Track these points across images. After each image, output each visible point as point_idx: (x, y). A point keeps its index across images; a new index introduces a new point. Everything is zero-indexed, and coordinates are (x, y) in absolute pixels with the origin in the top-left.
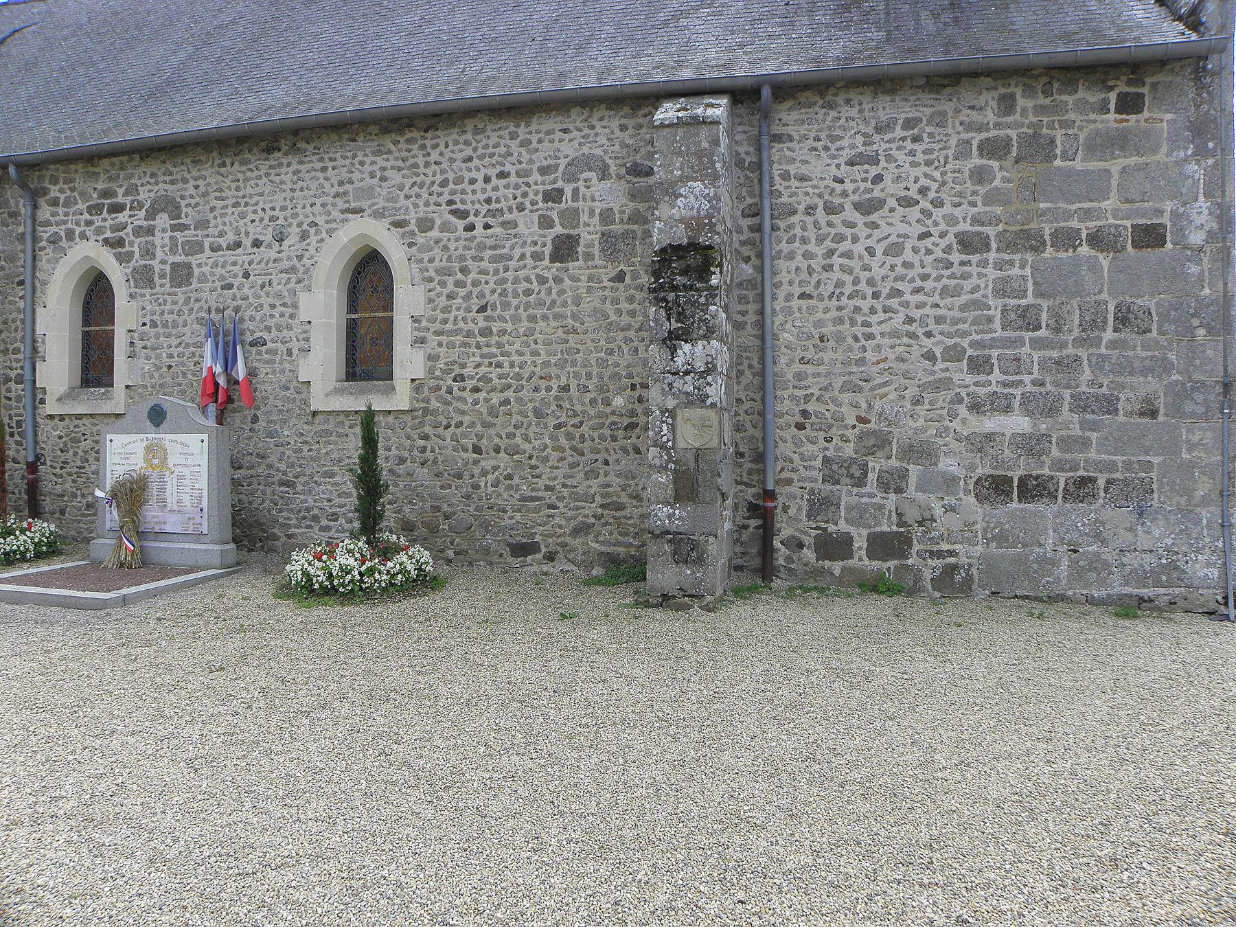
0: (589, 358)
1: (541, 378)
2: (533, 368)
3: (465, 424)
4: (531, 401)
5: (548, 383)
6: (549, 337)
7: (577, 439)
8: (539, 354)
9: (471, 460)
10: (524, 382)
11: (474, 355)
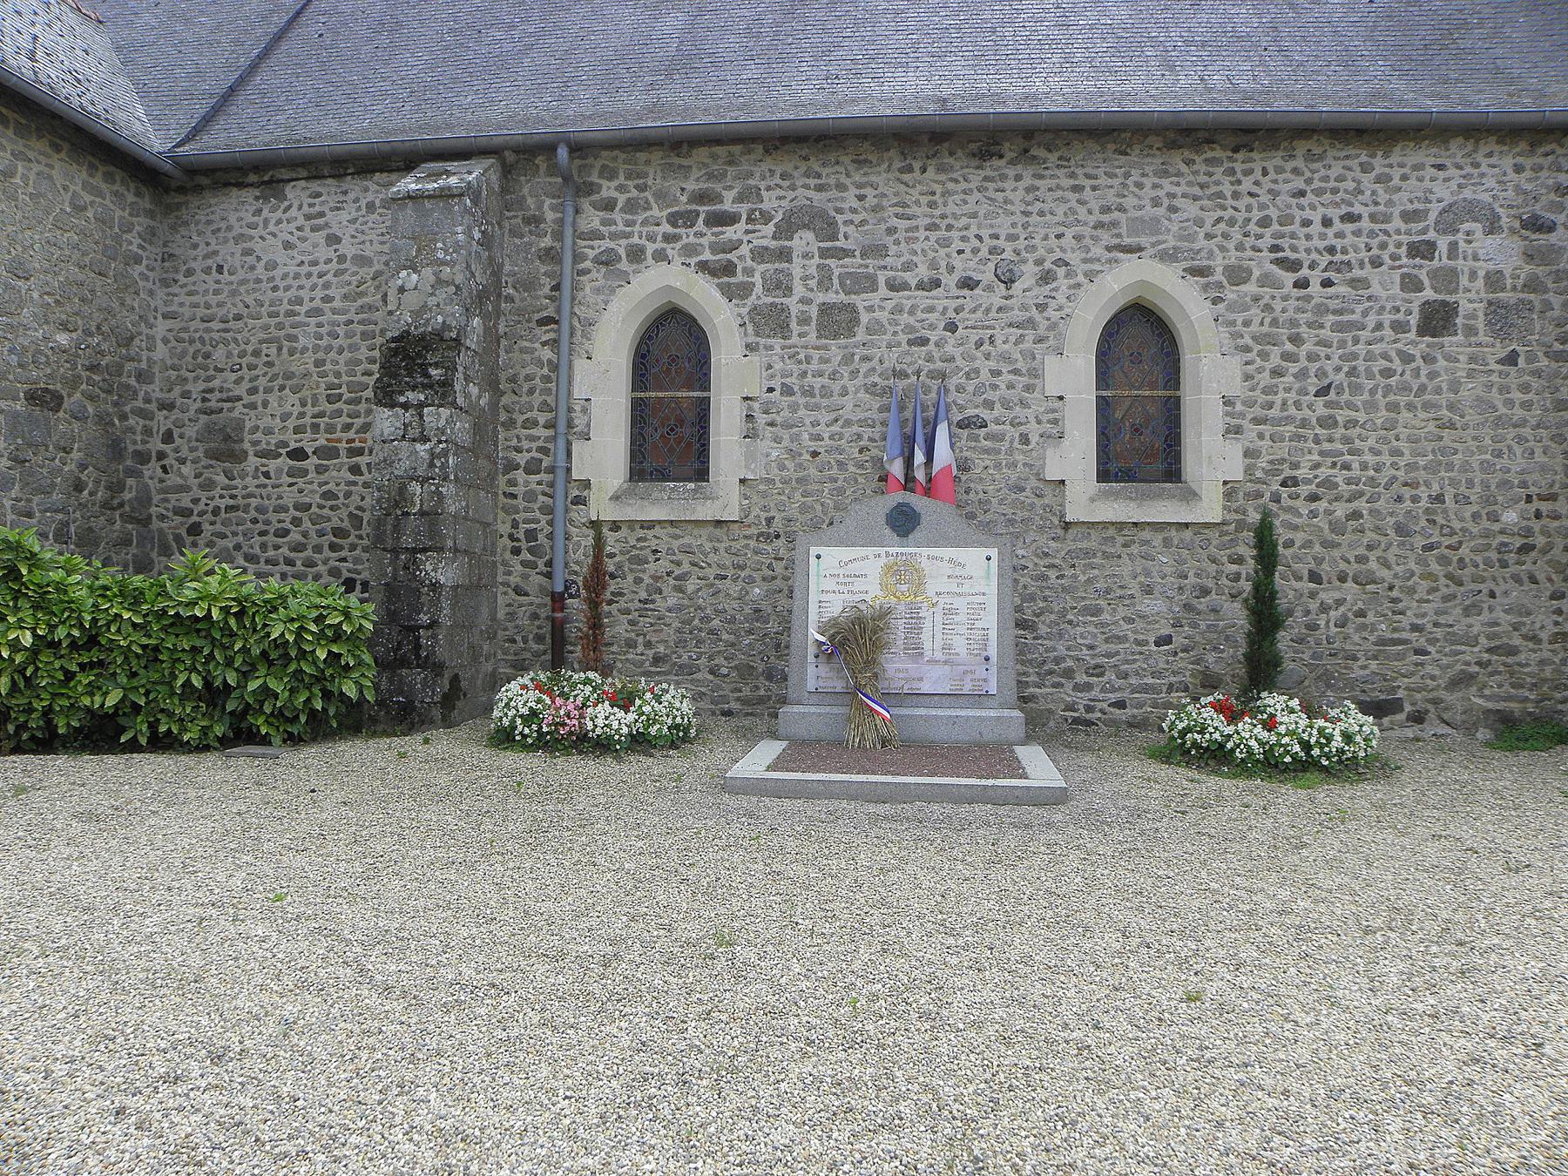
1: (1406, 484)
2: (1394, 472)
3: (1298, 544)
4: (1391, 514)
5: (1414, 492)
7: (1455, 564)
8: (1402, 454)
9: (1306, 591)
10: (1381, 489)
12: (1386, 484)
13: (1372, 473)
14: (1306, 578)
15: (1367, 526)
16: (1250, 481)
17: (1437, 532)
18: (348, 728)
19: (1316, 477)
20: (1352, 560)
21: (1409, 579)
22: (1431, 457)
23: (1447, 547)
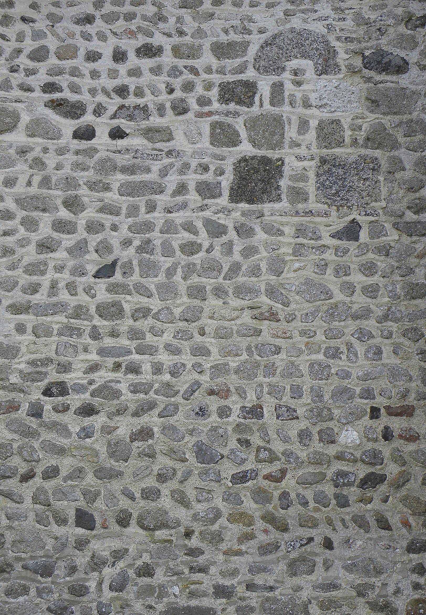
1: (211, 393)
2: (196, 376)
3: (64, 473)
4: (191, 432)
5: (223, 402)
6: (226, 324)
7: (276, 500)
8: (208, 353)
9: (72, 540)
10: (179, 399)
11: (86, 350)
12: (186, 392)
13: (167, 377)
14: (72, 518)
15: (158, 448)
17: (252, 457)
20: (138, 495)
22: (245, 356)
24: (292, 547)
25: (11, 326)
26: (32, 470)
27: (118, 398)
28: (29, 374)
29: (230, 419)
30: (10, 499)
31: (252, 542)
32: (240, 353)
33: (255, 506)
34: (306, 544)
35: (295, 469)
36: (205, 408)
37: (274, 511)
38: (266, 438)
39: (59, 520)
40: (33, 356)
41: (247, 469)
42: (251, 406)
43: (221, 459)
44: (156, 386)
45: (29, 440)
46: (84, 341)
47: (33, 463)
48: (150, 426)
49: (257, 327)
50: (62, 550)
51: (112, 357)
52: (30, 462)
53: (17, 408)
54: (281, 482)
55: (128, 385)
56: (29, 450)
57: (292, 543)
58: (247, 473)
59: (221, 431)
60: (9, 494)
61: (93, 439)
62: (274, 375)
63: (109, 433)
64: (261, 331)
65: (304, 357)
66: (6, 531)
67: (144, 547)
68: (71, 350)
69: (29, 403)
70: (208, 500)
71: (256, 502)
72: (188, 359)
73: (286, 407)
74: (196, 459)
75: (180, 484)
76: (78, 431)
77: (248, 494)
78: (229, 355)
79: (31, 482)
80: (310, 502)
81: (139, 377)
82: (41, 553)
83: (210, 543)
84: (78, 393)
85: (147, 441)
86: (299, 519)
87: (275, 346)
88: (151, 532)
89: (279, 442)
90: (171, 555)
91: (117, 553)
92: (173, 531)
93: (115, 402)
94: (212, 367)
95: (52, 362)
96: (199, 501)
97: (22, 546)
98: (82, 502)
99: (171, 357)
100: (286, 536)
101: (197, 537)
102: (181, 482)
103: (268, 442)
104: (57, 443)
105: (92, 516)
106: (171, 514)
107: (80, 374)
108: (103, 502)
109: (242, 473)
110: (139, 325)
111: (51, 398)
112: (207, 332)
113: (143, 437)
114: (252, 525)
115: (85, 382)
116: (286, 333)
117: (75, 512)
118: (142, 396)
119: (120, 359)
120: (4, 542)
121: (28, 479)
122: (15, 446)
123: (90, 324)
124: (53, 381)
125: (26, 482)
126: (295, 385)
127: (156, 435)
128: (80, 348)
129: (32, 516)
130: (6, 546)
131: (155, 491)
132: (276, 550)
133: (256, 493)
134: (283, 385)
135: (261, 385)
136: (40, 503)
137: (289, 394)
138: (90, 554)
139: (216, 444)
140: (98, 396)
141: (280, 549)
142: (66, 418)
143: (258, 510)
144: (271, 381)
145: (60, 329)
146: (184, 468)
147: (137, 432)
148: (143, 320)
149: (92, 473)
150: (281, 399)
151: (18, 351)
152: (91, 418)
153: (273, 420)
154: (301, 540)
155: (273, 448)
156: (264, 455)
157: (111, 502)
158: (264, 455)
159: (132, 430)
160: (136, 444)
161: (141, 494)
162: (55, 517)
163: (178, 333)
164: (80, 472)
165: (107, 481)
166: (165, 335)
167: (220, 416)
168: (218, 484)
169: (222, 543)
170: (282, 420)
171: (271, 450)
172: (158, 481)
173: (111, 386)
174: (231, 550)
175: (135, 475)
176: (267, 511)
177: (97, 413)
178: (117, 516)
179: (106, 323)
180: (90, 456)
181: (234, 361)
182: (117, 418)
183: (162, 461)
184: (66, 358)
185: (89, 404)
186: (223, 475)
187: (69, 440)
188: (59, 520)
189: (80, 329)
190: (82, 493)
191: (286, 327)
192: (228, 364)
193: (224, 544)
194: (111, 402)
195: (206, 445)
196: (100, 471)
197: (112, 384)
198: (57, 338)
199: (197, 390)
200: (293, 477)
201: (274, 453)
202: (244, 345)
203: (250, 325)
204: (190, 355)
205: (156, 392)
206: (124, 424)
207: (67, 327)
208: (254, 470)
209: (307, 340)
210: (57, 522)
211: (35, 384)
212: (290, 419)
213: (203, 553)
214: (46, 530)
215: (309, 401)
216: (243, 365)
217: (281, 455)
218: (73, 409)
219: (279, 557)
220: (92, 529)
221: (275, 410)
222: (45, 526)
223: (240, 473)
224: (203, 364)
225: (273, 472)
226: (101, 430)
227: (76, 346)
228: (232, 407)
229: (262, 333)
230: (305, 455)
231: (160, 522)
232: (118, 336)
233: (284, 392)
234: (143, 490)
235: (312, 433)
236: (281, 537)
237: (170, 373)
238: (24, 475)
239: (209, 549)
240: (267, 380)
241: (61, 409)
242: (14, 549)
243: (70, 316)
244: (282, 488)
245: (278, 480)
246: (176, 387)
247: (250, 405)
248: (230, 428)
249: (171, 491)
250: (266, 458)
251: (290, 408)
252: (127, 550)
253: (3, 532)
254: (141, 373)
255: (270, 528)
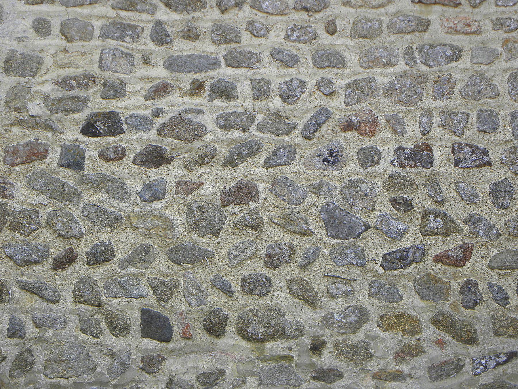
0: (490, 71)
1: (348, 126)
2: (323, 101)
3: (120, 254)
4: (317, 190)
5: (366, 142)
6: (371, 13)
7: (455, 295)
8: (340, 62)
9: (136, 357)
10: (296, 138)
11: (146, 61)
12: (307, 126)
13: (276, 103)
14: (136, 325)
15: (265, 215)
16: (20, 123)
17: (415, 227)
18: (151, 162)
19: (157, 113)
20: (236, 287)
21: (355, 327)
22: (402, 66)
23: (438, 259)
24: (482, 367)
25: (26, 24)
26: (71, 251)
27: (201, 138)
28: (60, 100)
29: (379, 168)
30: (38, 295)
31: (418, 360)
32: (393, 60)
33: (422, 304)
34: (506, 362)
35: (485, 245)
36: (337, 151)
37: (452, 312)
38: (438, 197)
39: (115, 327)
40: (64, 72)
41: (407, 246)
42: (412, 146)
43: (365, 231)
44: (260, 117)
45: (65, 205)
46: (143, 47)
47: (73, 240)
48: (252, 181)
49: (421, 16)
50: (122, 373)
51: (189, 72)
52: (68, 238)
53: (43, 155)
54: (464, 265)
55: (215, 117)
56: (65, 220)
57: (483, 361)
58: (408, 252)
59: (364, 187)
60: (37, 289)
61: (164, 201)
62: (450, 94)
63: (189, 192)
64: (428, 23)
65: (501, 64)
66: (34, 346)
67: (249, 367)
68: (123, 62)
69: (62, 147)
70: (346, 295)
71: (423, 298)
72: (309, 72)
73: (471, 146)
74: (325, 231)
75: (302, 270)
76: (140, 189)
77: (410, 285)
78: (376, 65)
79: (70, 270)
80: (510, 296)
81: (232, 103)
82: (91, 378)
83: (352, 360)
84: (138, 130)
85: (248, 204)
86: (494, 324)
87: (452, 47)
88: (258, 345)
89: (459, 203)
90: (292, 379)
91: (208, 376)
92: (293, 343)
93: (197, 144)
94: (349, 85)
95: (94, 81)
96: (332, 296)
97: (61, 368)
98: (151, 299)
99: (284, 71)
100: (473, 350)
101: (330, 352)
102: (303, 267)
103: (441, 203)
104: (109, 208)
105: (166, 320)
106: (289, 317)
107: (139, 100)
108: (183, 299)
109: (400, 252)
110: (230, 19)
111: (96, 139)
112: (339, 28)
113: (241, 198)
114: (417, 333)
115: (148, 112)
116: (469, 25)
117: (140, 315)
118: (238, 134)
119: (200, 76)
120: (33, 361)
121: (65, 264)
122: (43, 213)
123: (152, 18)
124: (97, 111)
125: (63, 269)
126: (485, 111)
127: (262, 196)
128: (138, 58)
129: (73, 322)
130: (35, 367)
131: (263, 281)
132: (457, 372)
133: (422, 284)
134: (466, 111)
135: (428, 113)
136: (85, 301)
137: (475, 125)
138: (166, 379)
139: (356, 208)
140: (169, 135)
141: (464, 370)
142: (382, 333)
143: (426, 310)
144: (445, 106)
145: (105, 28)
146: (307, 246)
147: (232, 190)
148: (236, 10)
149: (165, 255)
150: (463, 134)
151: (39, 63)
152: (160, 170)
153: (449, 168)
154: (497, 356)
155: (449, 213)
156: (433, 224)
157: (195, 299)
158: (433, 224)
159: (224, 187)
160: (231, 208)
161: (241, 285)
162: (109, 323)
163: (293, 30)
164: (146, 253)
165: (189, 266)
166: (272, 34)
167: (363, 163)
168: (362, 269)
169: (370, 361)
170: (464, 168)
171: (445, 215)
172: (267, 265)
173: (190, 120)
174: (386, 372)
175: (231, 256)
176: (442, 313)
177: (169, 161)
178: (205, 320)
179: (176, 16)
180: (160, 229)
181: (383, 75)
182: (200, 170)
183: (272, 234)
184: (116, 75)
185: (156, 148)
186: (369, 255)
187: (127, 204)
188: (115, 327)
189: (136, 27)
190: (150, 285)
191: (471, 16)
192: (374, 80)
193: (373, 363)
194: (190, 144)
195: (341, 210)
196: (177, 251)
197: (191, 116)
198: (99, 43)
199: (324, 122)
200: (483, 257)
201: (452, 220)
202: (400, 49)
203: (410, 14)
204: (312, 66)
205: (260, 128)
206: (212, 178)
207: (114, 24)
208: (418, 248)
209: (506, 35)
210: (112, 330)
211: (69, 116)
212: (478, 166)
213: (341, 376)
214: (96, 343)
215: (509, 136)
216: (398, 81)
217: (462, 224)
218: (130, 156)
219: (461, 383)
220: (167, 340)
221: (453, 152)
222: (95, 337)
223: (395, 252)
224: (334, 81)
225: (450, 250)
226: (177, 188)
227: (131, 55)
228: (381, 149)
229: (430, 27)
230: (503, 223)
231: (272, 329)
232: (197, 37)
233: (467, 122)
234: (244, 280)
235: (513, 188)
236: (464, 351)
237: (281, 96)
238: (59, 258)
239: (350, 370)
240: (439, 104)
241: (112, 155)
242: (49, 372)
243: (119, 6)
244: (465, 276)
245: (459, 263)
246: (291, 119)
247: (410, 145)
248: (378, 183)
249: (288, 281)
250: (437, 228)
251: (477, 148)
252: (222, 373)
253: (30, 346)
254: (236, 97)
255: (447, 337)
